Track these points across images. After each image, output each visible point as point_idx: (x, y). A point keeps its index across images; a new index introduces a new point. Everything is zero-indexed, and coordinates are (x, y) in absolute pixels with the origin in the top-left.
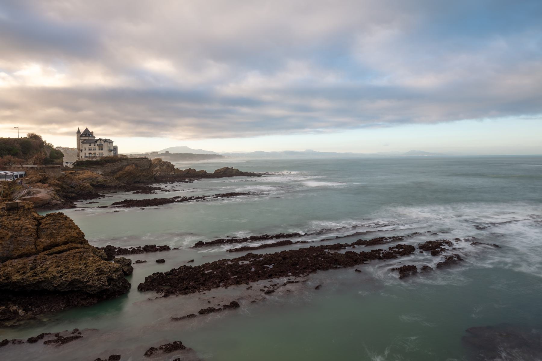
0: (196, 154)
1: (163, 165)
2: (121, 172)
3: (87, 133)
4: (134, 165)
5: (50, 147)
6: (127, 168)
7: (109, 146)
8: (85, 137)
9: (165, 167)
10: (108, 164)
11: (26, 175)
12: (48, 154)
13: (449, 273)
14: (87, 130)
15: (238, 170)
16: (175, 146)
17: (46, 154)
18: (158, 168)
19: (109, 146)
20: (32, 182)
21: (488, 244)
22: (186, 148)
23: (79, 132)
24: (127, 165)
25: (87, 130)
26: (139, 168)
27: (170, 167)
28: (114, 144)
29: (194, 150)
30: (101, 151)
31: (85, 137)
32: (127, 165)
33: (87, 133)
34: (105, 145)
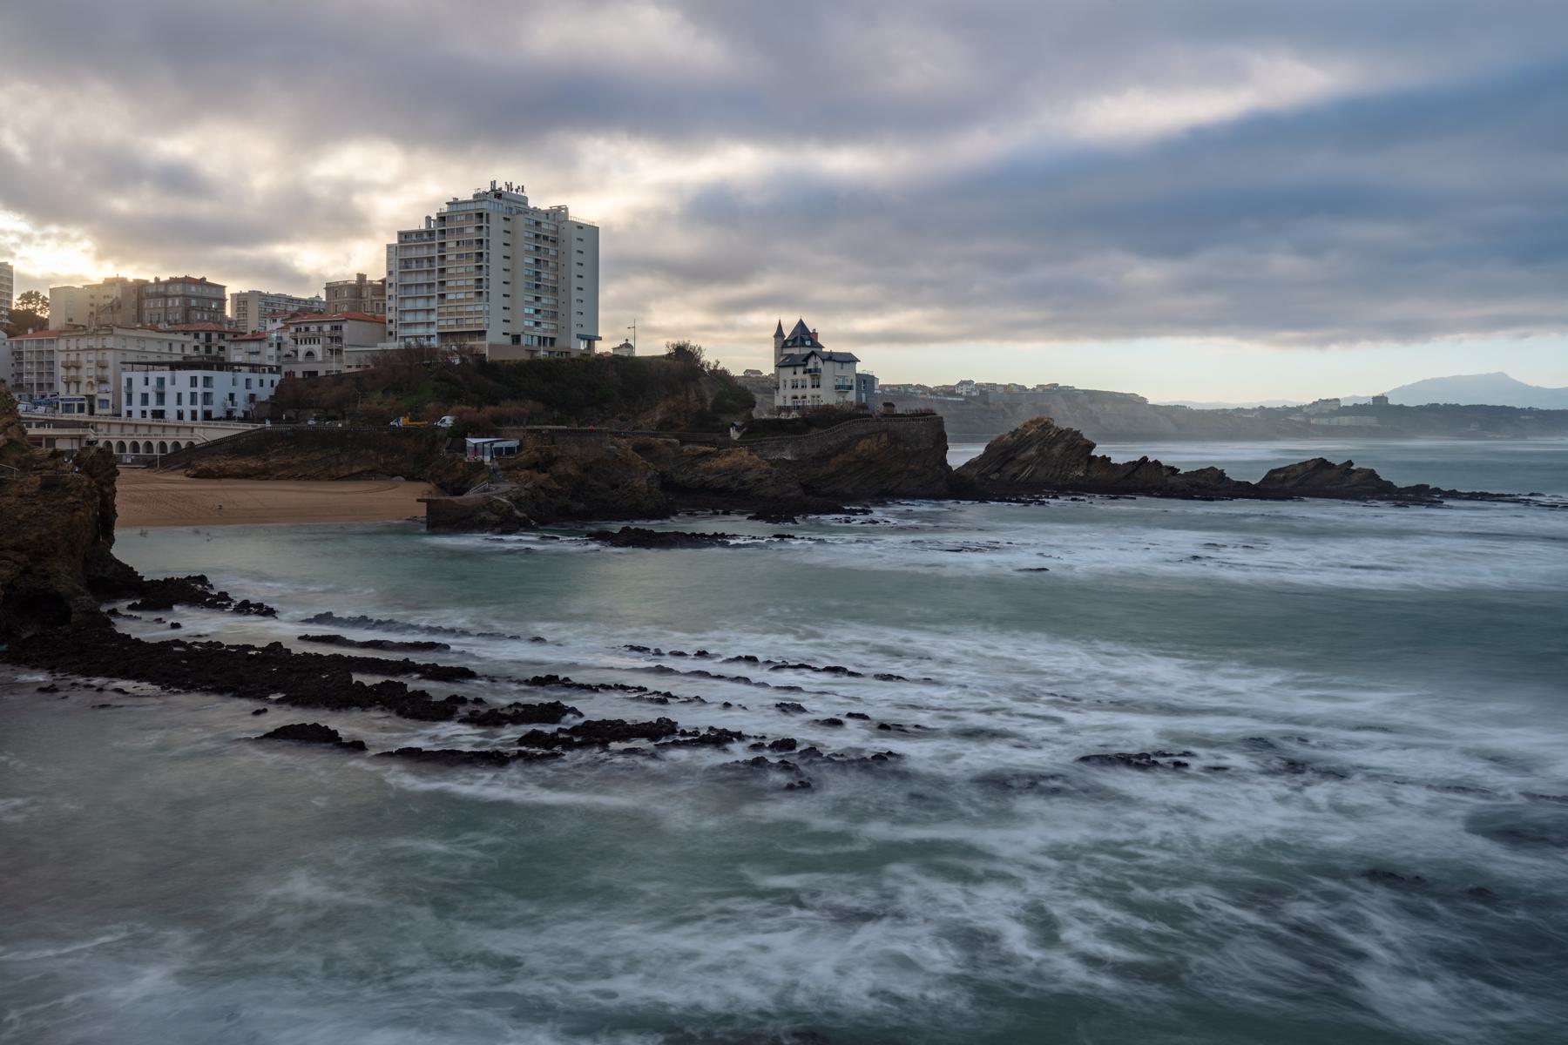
0: (1530, 411)
1: (1052, 443)
2: (841, 458)
3: (803, 335)
4: (884, 438)
5: (721, 377)
6: (863, 445)
7: (839, 372)
8: (799, 347)
9: (1057, 450)
10: (814, 431)
11: (520, 448)
12: (710, 401)
13: (1042, 838)
14: (801, 324)
15: (1372, 474)
16: (1484, 372)
17: (702, 400)
18: (1032, 452)
19: (839, 372)
20: (514, 467)
21: (751, 660)
22: (1501, 380)
23: (779, 332)
24: (862, 437)
25: (801, 324)
26: (901, 447)
27: (1079, 447)
28: (860, 368)
29: (1539, 391)
30: (816, 391)
31: (799, 347)
32: (862, 437)
33: (803, 335)
34: (827, 369)
